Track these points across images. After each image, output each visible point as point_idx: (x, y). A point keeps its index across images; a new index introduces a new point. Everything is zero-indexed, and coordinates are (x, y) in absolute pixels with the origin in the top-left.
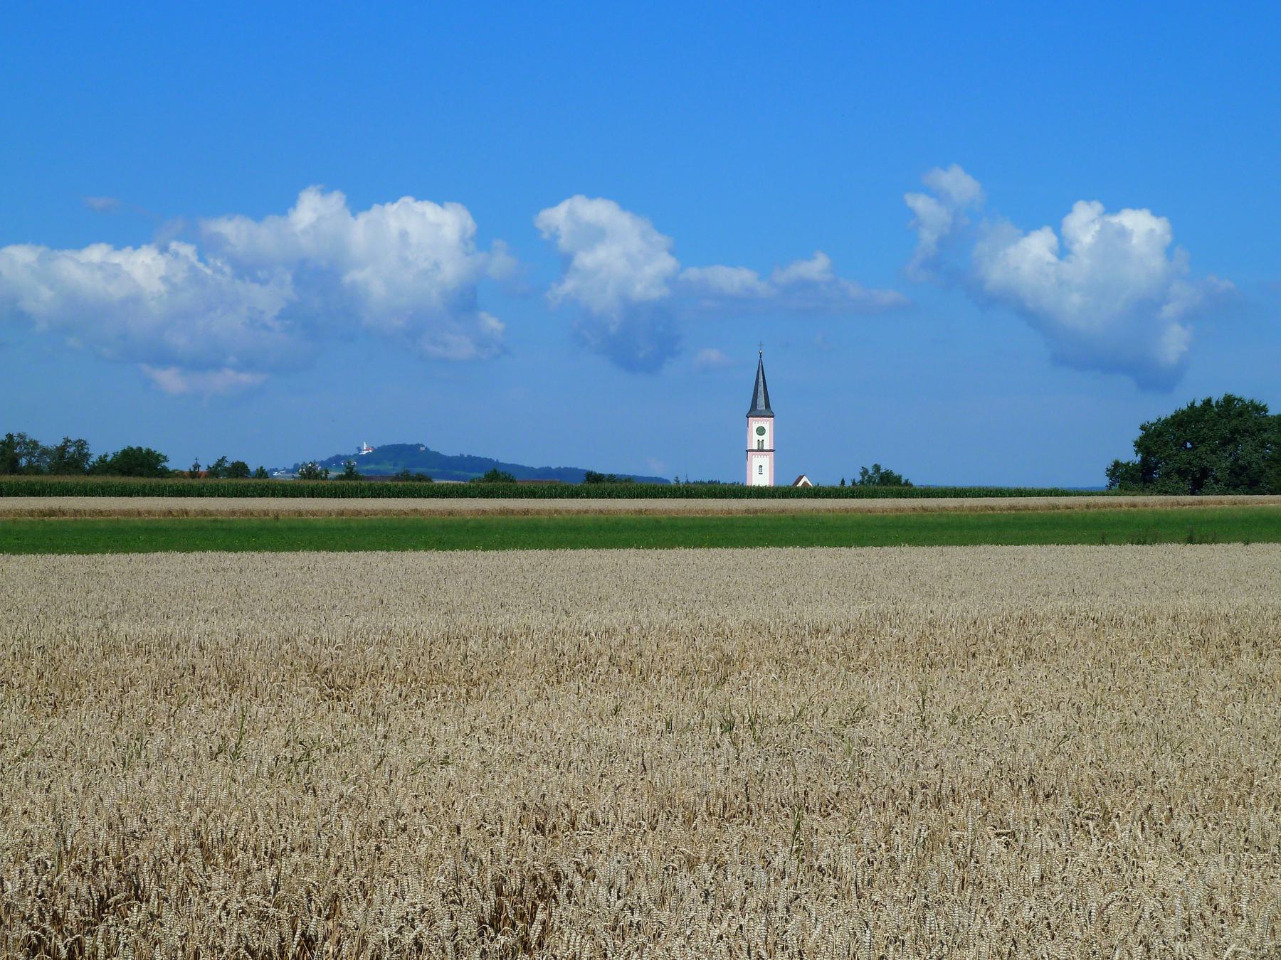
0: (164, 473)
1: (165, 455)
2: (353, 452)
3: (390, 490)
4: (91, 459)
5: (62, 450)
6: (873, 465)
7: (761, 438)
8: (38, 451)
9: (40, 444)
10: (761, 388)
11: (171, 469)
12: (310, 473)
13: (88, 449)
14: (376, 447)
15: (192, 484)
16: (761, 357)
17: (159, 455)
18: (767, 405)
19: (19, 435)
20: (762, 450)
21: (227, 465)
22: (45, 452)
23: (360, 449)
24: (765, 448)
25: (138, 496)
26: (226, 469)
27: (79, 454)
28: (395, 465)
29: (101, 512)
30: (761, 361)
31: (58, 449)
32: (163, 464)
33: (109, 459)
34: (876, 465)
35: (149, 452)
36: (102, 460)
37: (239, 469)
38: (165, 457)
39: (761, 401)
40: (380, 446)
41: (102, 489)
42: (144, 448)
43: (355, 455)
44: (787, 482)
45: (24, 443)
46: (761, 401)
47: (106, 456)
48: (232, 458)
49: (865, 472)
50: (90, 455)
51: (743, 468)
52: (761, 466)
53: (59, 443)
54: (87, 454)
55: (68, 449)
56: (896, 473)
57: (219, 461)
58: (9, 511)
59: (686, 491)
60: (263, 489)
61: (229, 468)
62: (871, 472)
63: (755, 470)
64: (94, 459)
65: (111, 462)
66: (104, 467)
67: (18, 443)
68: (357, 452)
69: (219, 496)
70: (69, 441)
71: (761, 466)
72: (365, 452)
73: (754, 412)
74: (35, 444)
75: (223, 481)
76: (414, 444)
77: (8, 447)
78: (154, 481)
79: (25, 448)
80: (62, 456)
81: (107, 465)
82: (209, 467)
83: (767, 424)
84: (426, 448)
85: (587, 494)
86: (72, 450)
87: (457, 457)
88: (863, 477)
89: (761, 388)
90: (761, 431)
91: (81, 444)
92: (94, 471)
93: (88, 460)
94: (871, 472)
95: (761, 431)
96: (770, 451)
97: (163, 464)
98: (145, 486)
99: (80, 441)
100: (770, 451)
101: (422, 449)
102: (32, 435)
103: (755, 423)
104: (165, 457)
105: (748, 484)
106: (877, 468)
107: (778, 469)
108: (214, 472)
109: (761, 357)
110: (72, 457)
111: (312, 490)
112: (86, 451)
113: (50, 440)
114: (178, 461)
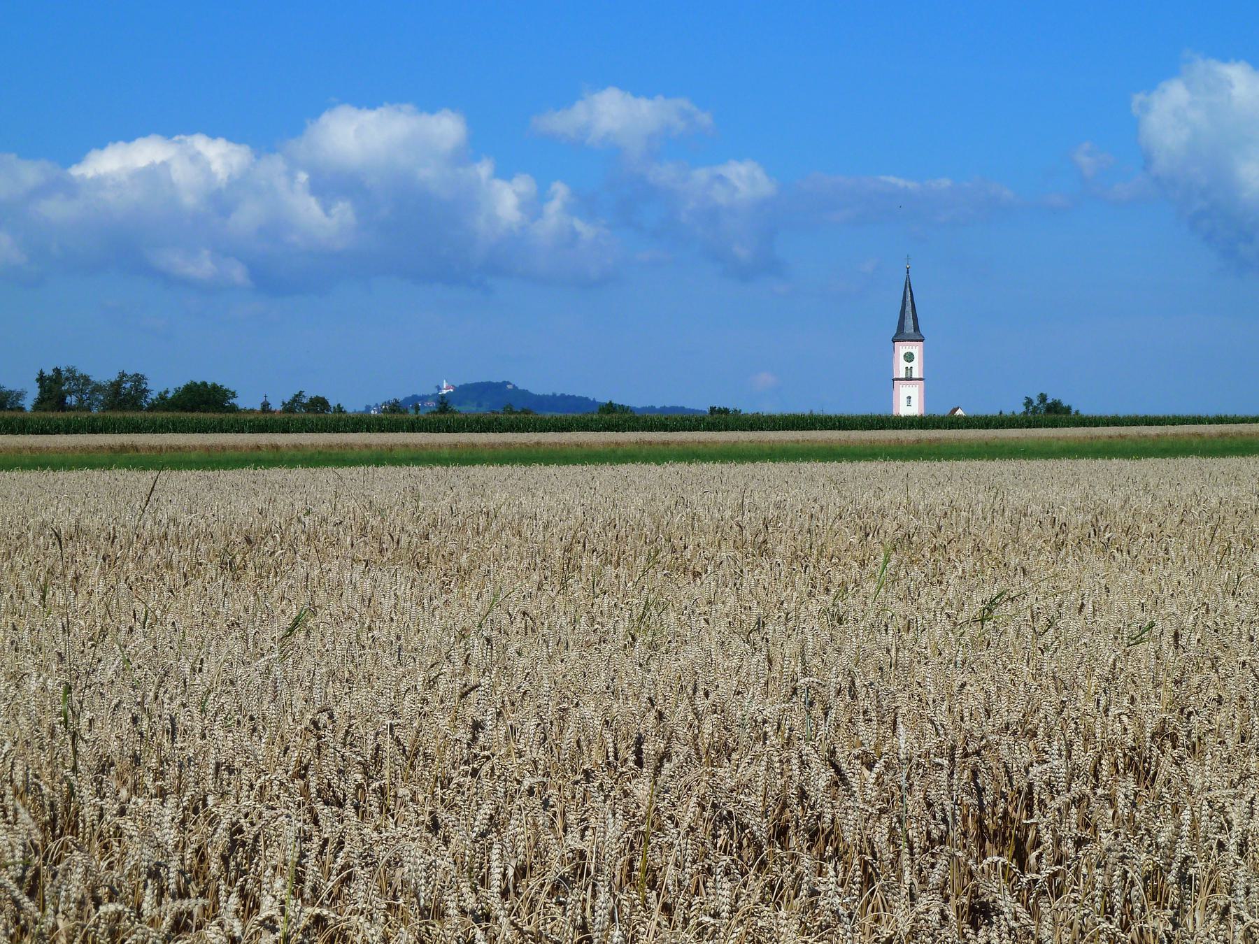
0: (233, 409)
1: (232, 390)
2: (431, 391)
3: (500, 424)
4: (151, 396)
5: (117, 386)
6: (1038, 394)
7: (909, 365)
8: (90, 387)
9: (92, 379)
10: (909, 308)
11: (241, 407)
12: (395, 407)
13: (146, 384)
14: (457, 385)
15: (264, 422)
16: (908, 273)
17: (226, 390)
18: (916, 328)
19: (68, 370)
20: (911, 379)
21: (305, 401)
22: (98, 388)
23: (439, 388)
24: (913, 377)
25: (215, 432)
26: (304, 406)
27: (136, 389)
28: (480, 405)
29: (180, 448)
30: (908, 277)
31: (112, 384)
32: (231, 401)
33: (170, 396)
34: (1041, 394)
35: (214, 387)
36: (162, 397)
37: (319, 404)
38: (234, 393)
39: (909, 322)
40: (462, 384)
41: (173, 425)
42: (209, 383)
43: (434, 395)
44: (943, 411)
45: (74, 378)
46: (909, 322)
47: (167, 392)
48: (310, 393)
49: (1029, 402)
50: (148, 391)
51: (889, 398)
52: (909, 398)
53: (114, 377)
54: (145, 390)
55: (124, 385)
56: (1065, 404)
57: (296, 396)
58: (74, 447)
59: (839, 421)
60: (356, 424)
61: (306, 404)
62: (1036, 402)
63: (903, 401)
64: (154, 396)
65: (171, 399)
66: (164, 403)
67: (67, 379)
68: (436, 391)
69: (306, 432)
70: (124, 375)
71: (909, 398)
72: (445, 392)
73: (900, 336)
74: (86, 380)
75: (300, 414)
76: (501, 381)
77: (56, 383)
78: (217, 416)
79: (75, 384)
80: (117, 393)
81: (168, 403)
82: (284, 403)
83: (916, 349)
84: (514, 386)
85: (726, 426)
86: (128, 385)
87: (548, 396)
88: (1027, 408)
89: (909, 308)
90: (909, 357)
91: (138, 379)
92: (153, 408)
93: (146, 397)
94: (1036, 402)
95: (909, 357)
96: (920, 379)
97: (231, 401)
98: (222, 420)
99: (137, 375)
100: (920, 379)
101: (509, 387)
102: (82, 370)
103: (902, 348)
104: (234, 393)
105: (895, 413)
106: (1043, 398)
107: (928, 397)
108: (289, 408)
109: (908, 273)
110: (129, 393)
111: (413, 425)
112: (144, 386)
113: (103, 375)
114: (247, 400)
